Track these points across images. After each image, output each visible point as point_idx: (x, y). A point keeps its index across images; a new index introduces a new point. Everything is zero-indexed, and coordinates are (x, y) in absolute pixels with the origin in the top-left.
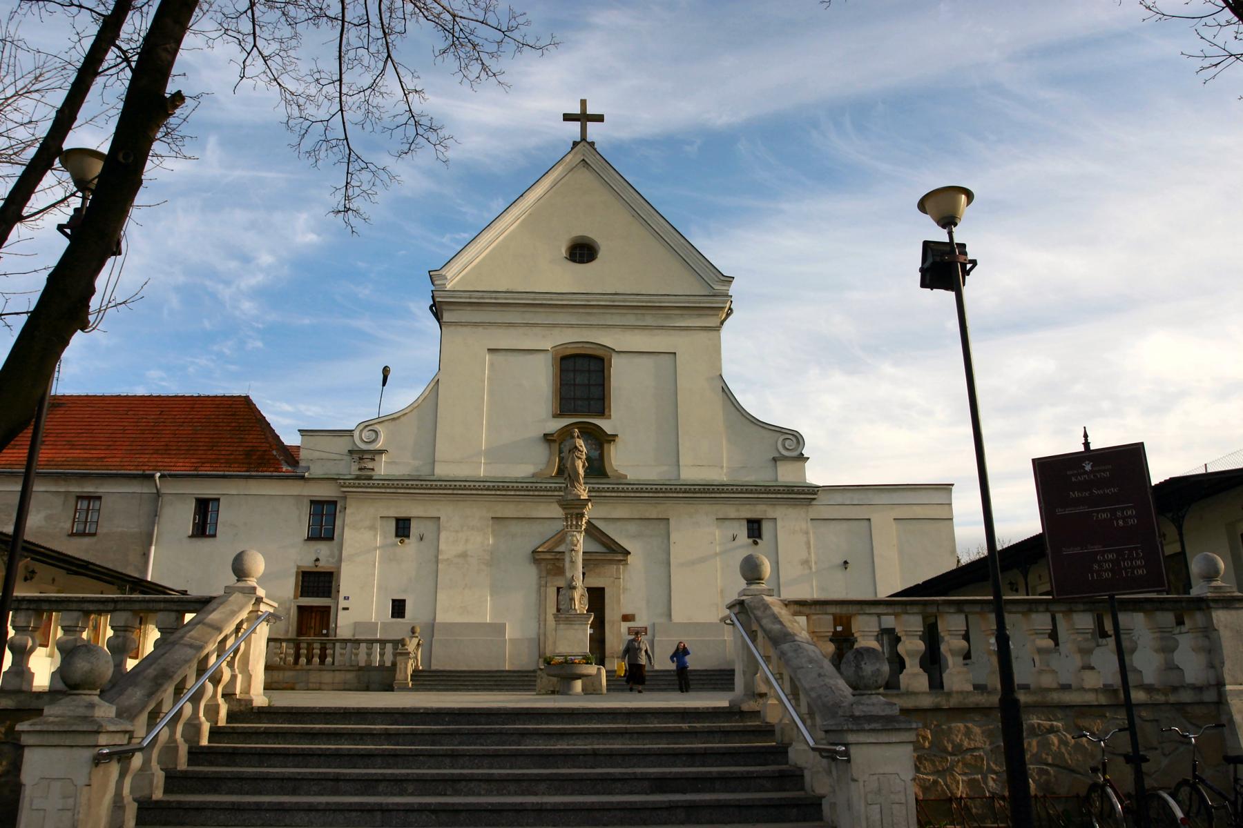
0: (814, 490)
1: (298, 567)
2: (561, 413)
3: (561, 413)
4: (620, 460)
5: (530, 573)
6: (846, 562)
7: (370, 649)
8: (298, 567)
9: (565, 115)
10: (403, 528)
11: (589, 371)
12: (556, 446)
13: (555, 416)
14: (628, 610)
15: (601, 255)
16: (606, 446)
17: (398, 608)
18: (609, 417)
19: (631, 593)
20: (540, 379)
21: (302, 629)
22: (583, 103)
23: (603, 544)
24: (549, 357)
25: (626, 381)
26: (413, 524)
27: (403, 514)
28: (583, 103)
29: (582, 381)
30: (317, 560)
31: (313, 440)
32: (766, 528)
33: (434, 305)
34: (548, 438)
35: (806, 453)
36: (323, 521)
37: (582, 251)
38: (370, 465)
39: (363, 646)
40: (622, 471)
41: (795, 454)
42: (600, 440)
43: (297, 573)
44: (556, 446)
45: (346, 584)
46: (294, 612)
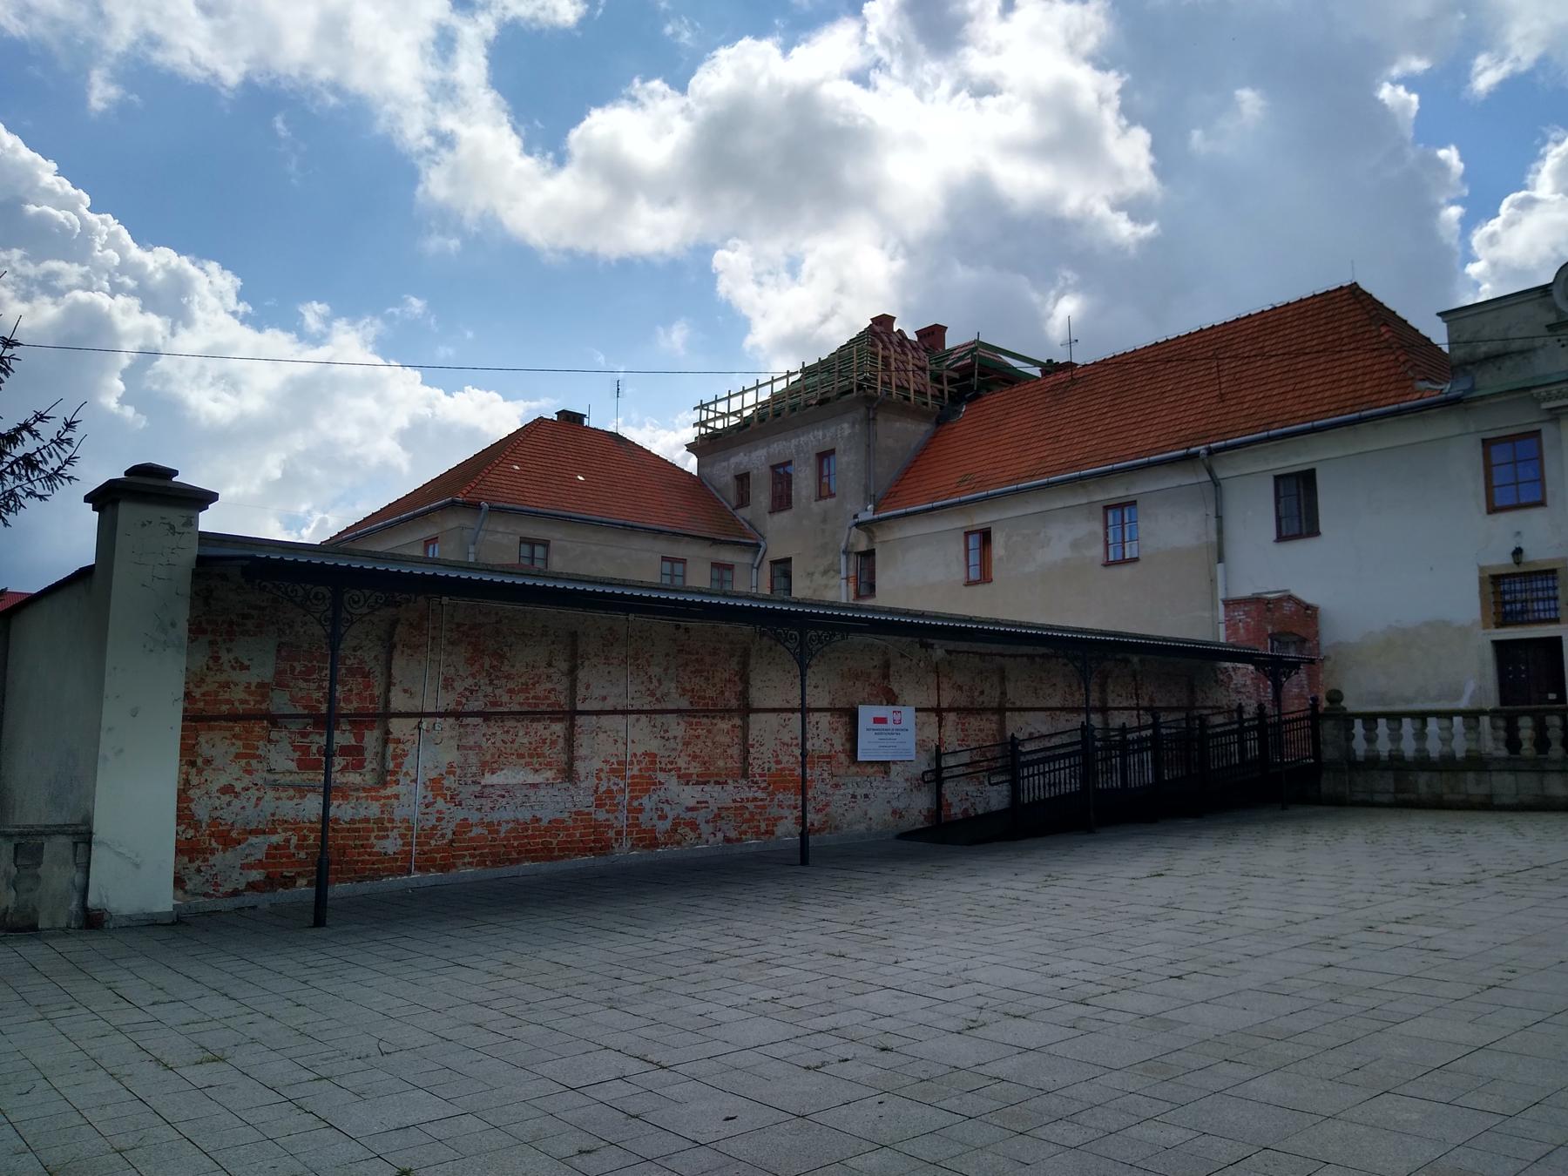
1: (1482, 569)
8: (1482, 569)
30: (1518, 552)
46: (1489, 654)
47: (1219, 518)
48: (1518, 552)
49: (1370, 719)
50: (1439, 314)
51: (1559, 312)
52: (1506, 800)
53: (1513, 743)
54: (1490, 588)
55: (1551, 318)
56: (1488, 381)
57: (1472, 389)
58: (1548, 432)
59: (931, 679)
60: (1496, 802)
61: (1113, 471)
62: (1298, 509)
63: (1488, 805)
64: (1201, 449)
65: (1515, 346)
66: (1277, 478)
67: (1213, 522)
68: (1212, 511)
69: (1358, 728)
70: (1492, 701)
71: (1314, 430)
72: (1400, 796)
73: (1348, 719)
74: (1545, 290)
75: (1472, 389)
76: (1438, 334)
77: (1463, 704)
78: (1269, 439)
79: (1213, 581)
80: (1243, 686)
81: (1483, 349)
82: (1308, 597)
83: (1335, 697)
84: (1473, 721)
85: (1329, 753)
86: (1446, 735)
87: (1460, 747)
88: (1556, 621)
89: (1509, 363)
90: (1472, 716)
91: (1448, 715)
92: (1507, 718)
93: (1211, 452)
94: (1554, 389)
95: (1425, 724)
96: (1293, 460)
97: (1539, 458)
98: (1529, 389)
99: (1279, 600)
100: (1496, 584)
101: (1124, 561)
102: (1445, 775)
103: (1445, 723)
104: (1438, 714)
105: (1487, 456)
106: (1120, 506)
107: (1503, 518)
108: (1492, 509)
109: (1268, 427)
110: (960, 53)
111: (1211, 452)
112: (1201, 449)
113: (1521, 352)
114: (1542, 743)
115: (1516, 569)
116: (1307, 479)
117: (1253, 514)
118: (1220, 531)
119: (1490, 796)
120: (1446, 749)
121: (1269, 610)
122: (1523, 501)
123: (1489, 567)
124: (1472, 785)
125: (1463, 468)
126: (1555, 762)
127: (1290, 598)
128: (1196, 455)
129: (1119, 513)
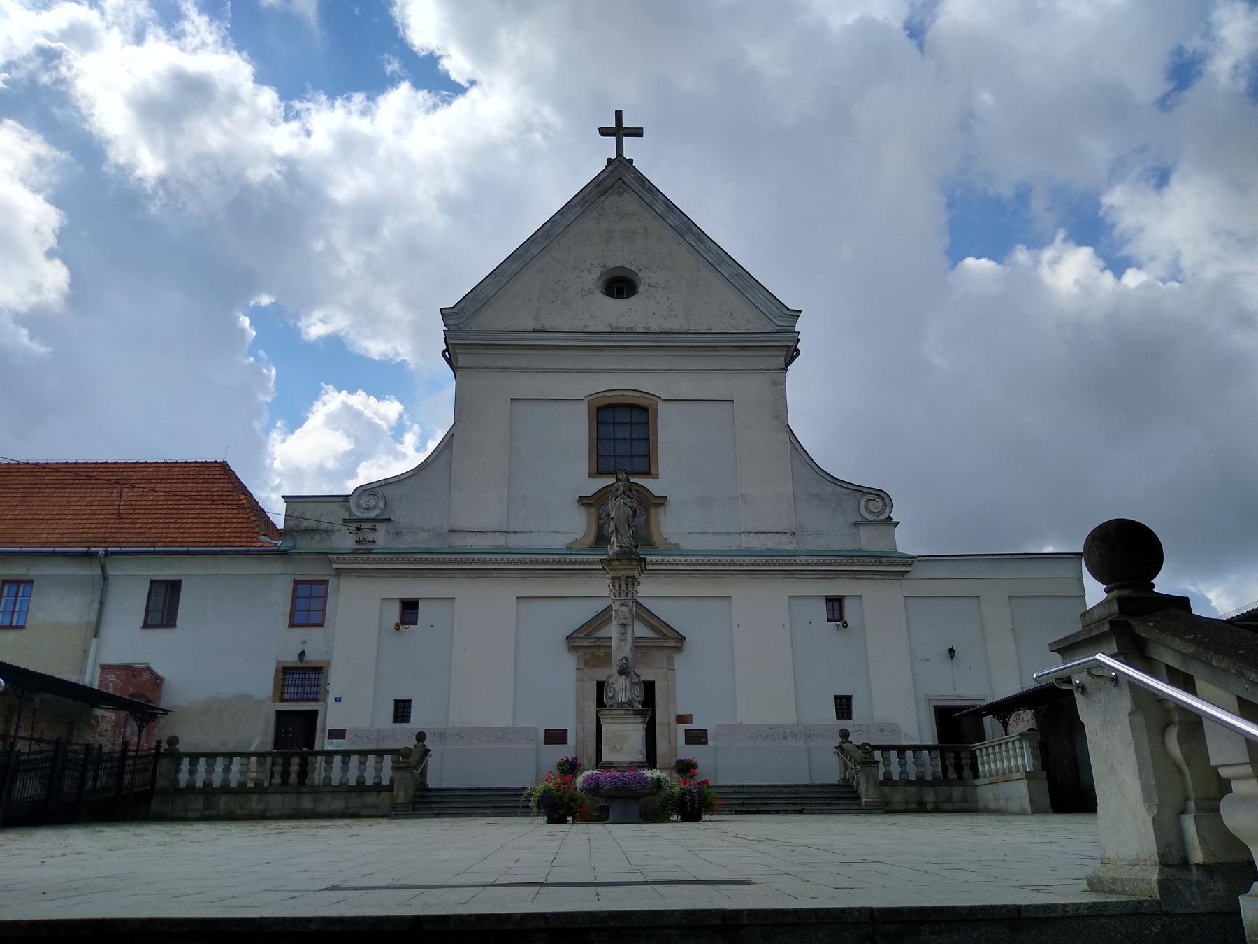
0: (910, 560)
1: (278, 663)
2: (597, 472)
3: (597, 472)
4: (673, 527)
5: (568, 664)
6: (951, 651)
7: (362, 763)
8: (278, 663)
9: (641, 135)
10: (835, 606)
11: (631, 424)
12: (593, 510)
13: (591, 476)
15: (642, 288)
16: (652, 510)
18: (656, 477)
19: (690, 690)
20: (576, 431)
21: (280, 739)
22: (619, 115)
23: (653, 628)
24: (583, 408)
25: (671, 432)
26: (422, 608)
27: (410, 594)
28: (619, 115)
29: (623, 432)
30: (302, 654)
32: (849, 609)
33: (447, 350)
34: (583, 501)
36: (307, 608)
37: (620, 285)
38: (370, 536)
41: (883, 517)
42: (650, 503)
43: (277, 670)
44: (593, 510)
45: (336, 683)
46: (272, 719)
47: (102, 603)
48: (302, 654)
49: (194, 757)
51: (352, 513)
53: (285, 775)
54: (281, 676)
55: (347, 516)
56: (304, 544)
57: (294, 547)
58: (333, 582)
61: (20, 553)
62: (163, 606)
64: (101, 551)
66: (152, 582)
67: (96, 606)
68: (97, 598)
69: (185, 764)
70: (269, 747)
71: (188, 553)
72: (206, 813)
73: (177, 757)
75: (294, 547)
76: (277, 513)
78: (154, 553)
79: (86, 652)
80: (107, 729)
81: (305, 524)
82: (160, 671)
83: (173, 741)
85: (161, 782)
86: (244, 769)
88: (317, 700)
89: (318, 537)
93: (107, 554)
95: (231, 762)
96: (167, 571)
98: (328, 554)
99: (142, 670)
100: (285, 672)
101: (10, 627)
103: (245, 760)
105: (295, 590)
106: (18, 582)
107: (298, 631)
108: (292, 625)
109: (154, 544)
110: (78, 94)
111: (107, 554)
112: (101, 551)
113: (326, 531)
116: (173, 588)
117: (129, 601)
118: (100, 614)
121: (134, 676)
124: (255, 804)
125: (280, 597)
127: (149, 670)
128: (97, 553)
129: (14, 588)
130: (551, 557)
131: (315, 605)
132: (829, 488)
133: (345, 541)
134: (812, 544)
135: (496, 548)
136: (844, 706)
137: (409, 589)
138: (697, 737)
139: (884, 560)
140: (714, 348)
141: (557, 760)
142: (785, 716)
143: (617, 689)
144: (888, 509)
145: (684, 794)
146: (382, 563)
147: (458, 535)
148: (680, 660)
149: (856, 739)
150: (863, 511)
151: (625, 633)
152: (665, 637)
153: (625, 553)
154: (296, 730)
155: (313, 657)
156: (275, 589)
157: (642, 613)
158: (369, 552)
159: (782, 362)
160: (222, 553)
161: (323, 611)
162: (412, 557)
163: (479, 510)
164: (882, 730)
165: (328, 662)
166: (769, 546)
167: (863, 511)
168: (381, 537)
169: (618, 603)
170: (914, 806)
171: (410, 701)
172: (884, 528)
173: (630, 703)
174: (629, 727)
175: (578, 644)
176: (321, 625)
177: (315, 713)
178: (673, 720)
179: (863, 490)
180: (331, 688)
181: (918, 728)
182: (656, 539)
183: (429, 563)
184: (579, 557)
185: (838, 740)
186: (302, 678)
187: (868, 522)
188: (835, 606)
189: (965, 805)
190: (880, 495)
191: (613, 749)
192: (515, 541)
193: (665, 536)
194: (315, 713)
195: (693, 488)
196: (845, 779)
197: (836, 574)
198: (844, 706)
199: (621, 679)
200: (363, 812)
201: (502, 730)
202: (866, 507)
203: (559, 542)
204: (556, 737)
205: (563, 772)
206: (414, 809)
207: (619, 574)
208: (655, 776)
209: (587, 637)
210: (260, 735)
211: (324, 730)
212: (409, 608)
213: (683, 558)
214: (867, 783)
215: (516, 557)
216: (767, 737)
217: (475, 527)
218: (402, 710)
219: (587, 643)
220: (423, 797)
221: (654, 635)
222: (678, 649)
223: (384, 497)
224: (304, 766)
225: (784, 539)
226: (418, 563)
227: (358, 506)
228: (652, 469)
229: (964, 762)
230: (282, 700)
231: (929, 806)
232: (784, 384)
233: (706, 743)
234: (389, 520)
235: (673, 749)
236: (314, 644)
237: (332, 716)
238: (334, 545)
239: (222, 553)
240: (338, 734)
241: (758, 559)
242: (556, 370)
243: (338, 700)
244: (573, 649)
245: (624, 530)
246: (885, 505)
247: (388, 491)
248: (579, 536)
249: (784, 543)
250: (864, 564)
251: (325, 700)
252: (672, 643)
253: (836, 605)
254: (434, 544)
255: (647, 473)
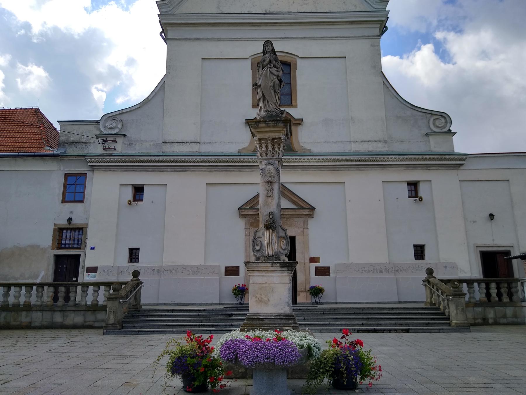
0: (464, 157)
1: (55, 225)
4: (305, 138)
5: (241, 224)
6: (492, 216)
8: (55, 225)
10: (413, 186)
14: (313, 254)
17: (134, 255)
18: (296, 107)
19: (318, 241)
20: (243, 76)
23: (294, 202)
25: (305, 78)
27: (138, 182)
29: (276, 75)
30: (70, 220)
31: (69, 128)
32: (422, 190)
33: (163, 32)
34: (248, 122)
35: (453, 129)
36: (74, 189)
39: (91, 288)
40: (306, 146)
41: (446, 130)
43: (55, 230)
45: (91, 238)
46: (52, 260)
48: (70, 220)
50: (58, 122)
51: (101, 131)
52: (37, 324)
53: (488, 295)
54: (57, 233)
56: (71, 151)
58: (89, 174)
59: (514, 285)
60: (33, 325)
63: (29, 327)
65: (83, 140)
74: (97, 122)
75: (65, 152)
77: (38, 281)
84: (29, 289)
86: (17, 294)
87: (22, 300)
88: (80, 248)
89: (80, 146)
90: (41, 286)
91: (20, 286)
92: (55, 286)
94: (93, 158)
97: (84, 184)
100: (60, 231)
102: (13, 313)
103: (18, 289)
104: (15, 285)
105: (65, 180)
107: (67, 205)
108: (64, 201)
113: (85, 143)
114: (499, 294)
115: (68, 227)
119: (30, 323)
120: (17, 301)
122: (77, 199)
123: (59, 224)
124: (24, 318)
126: (59, 307)
130: (228, 158)
131: (79, 189)
132: (409, 112)
133: (96, 149)
134: (398, 148)
135: (193, 152)
136: (419, 252)
137: (138, 179)
138: (323, 272)
139: (447, 157)
140: (333, 23)
141: (232, 286)
142: (381, 258)
143: (264, 243)
144: (448, 125)
145: (337, 359)
146: (119, 162)
147: (168, 145)
148: (311, 223)
149: (439, 275)
150: (432, 126)
151: (271, 190)
152: (302, 208)
153: (271, 116)
154: (67, 268)
155: (77, 221)
156: (51, 179)
157: (285, 192)
158: (110, 155)
159: (377, 32)
160: (18, 156)
161: (84, 193)
162: (138, 158)
163: (182, 130)
164: (446, 267)
165: (87, 225)
166: (370, 149)
167: (432, 126)
168: (120, 146)
169: (264, 163)
170: (480, 321)
171: (139, 249)
172: (447, 137)
173: (276, 256)
174: (276, 279)
175: (246, 213)
176: (82, 202)
177: (79, 256)
178: (307, 261)
179: (431, 113)
180: (88, 241)
181: (470, 268)
182: (296, 146)
183: (149, 162)
184: (246, 158)
185: (425, 276)
186: (70, 235)
187: (435, 133)
188: (413, 186)
189: (515, 320)
190: (444, 116)
191: (260, 301)
192: (205, 149)
193: (302, 144)
194: (79, 256)
195: (321, 111)
196: (432, 304)
197: (415, 167)
198: (419, 252)
199: (267, 233)
200: (96, 324)
201: (197, 267)
202: (434, 124)
203: (234, 149)
204: (232, 271)
205: (236, 295)
206: (123, 327)
207: (266, 136)
208: (305, 342)
209: (251, 208)
210: (44, 271)
211: (83, 267)
212: (138, 190)
213: (313, 157)
214: (457, 309)
215: (205, 158)
216: (369, 271)
217: (179, 139)
218: (134, 255)
219: (249, 210)
220: (133, 316)
221: (294, 207)
222: (311, 216)
223: (122, 121)
224: (68, 292)
225: (380, 145)
226: (142, 162)
227: (105, 127)
228: (293, 102)
229: (502, 290)
230: (59, 248)
231: (491, 321)
232: (378, 45)
233: (329, 275)
234: (125, 135)
235: (308, 279)
236: (77, 213)
237: (89, 259)
238: (90, 152)
239: (18, 156)
240: (93, 270)
241: (363, 157)
242: (231, 39)
243: (93, 248)
244: (242, 216)
245: (275, 123)
246: (446, 122)
247: (124, 117)
248: (246, 145)
249: (380, 148)
250: (433, 160)
251: (85, 248)
252: (307, 212)
253: (413, 187)
254: (153, 151)
255: (290, 105)
